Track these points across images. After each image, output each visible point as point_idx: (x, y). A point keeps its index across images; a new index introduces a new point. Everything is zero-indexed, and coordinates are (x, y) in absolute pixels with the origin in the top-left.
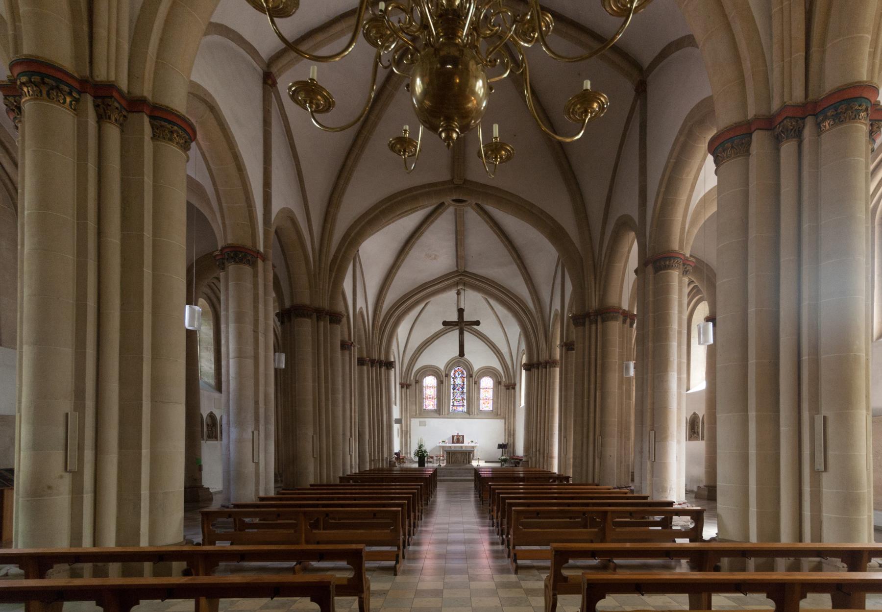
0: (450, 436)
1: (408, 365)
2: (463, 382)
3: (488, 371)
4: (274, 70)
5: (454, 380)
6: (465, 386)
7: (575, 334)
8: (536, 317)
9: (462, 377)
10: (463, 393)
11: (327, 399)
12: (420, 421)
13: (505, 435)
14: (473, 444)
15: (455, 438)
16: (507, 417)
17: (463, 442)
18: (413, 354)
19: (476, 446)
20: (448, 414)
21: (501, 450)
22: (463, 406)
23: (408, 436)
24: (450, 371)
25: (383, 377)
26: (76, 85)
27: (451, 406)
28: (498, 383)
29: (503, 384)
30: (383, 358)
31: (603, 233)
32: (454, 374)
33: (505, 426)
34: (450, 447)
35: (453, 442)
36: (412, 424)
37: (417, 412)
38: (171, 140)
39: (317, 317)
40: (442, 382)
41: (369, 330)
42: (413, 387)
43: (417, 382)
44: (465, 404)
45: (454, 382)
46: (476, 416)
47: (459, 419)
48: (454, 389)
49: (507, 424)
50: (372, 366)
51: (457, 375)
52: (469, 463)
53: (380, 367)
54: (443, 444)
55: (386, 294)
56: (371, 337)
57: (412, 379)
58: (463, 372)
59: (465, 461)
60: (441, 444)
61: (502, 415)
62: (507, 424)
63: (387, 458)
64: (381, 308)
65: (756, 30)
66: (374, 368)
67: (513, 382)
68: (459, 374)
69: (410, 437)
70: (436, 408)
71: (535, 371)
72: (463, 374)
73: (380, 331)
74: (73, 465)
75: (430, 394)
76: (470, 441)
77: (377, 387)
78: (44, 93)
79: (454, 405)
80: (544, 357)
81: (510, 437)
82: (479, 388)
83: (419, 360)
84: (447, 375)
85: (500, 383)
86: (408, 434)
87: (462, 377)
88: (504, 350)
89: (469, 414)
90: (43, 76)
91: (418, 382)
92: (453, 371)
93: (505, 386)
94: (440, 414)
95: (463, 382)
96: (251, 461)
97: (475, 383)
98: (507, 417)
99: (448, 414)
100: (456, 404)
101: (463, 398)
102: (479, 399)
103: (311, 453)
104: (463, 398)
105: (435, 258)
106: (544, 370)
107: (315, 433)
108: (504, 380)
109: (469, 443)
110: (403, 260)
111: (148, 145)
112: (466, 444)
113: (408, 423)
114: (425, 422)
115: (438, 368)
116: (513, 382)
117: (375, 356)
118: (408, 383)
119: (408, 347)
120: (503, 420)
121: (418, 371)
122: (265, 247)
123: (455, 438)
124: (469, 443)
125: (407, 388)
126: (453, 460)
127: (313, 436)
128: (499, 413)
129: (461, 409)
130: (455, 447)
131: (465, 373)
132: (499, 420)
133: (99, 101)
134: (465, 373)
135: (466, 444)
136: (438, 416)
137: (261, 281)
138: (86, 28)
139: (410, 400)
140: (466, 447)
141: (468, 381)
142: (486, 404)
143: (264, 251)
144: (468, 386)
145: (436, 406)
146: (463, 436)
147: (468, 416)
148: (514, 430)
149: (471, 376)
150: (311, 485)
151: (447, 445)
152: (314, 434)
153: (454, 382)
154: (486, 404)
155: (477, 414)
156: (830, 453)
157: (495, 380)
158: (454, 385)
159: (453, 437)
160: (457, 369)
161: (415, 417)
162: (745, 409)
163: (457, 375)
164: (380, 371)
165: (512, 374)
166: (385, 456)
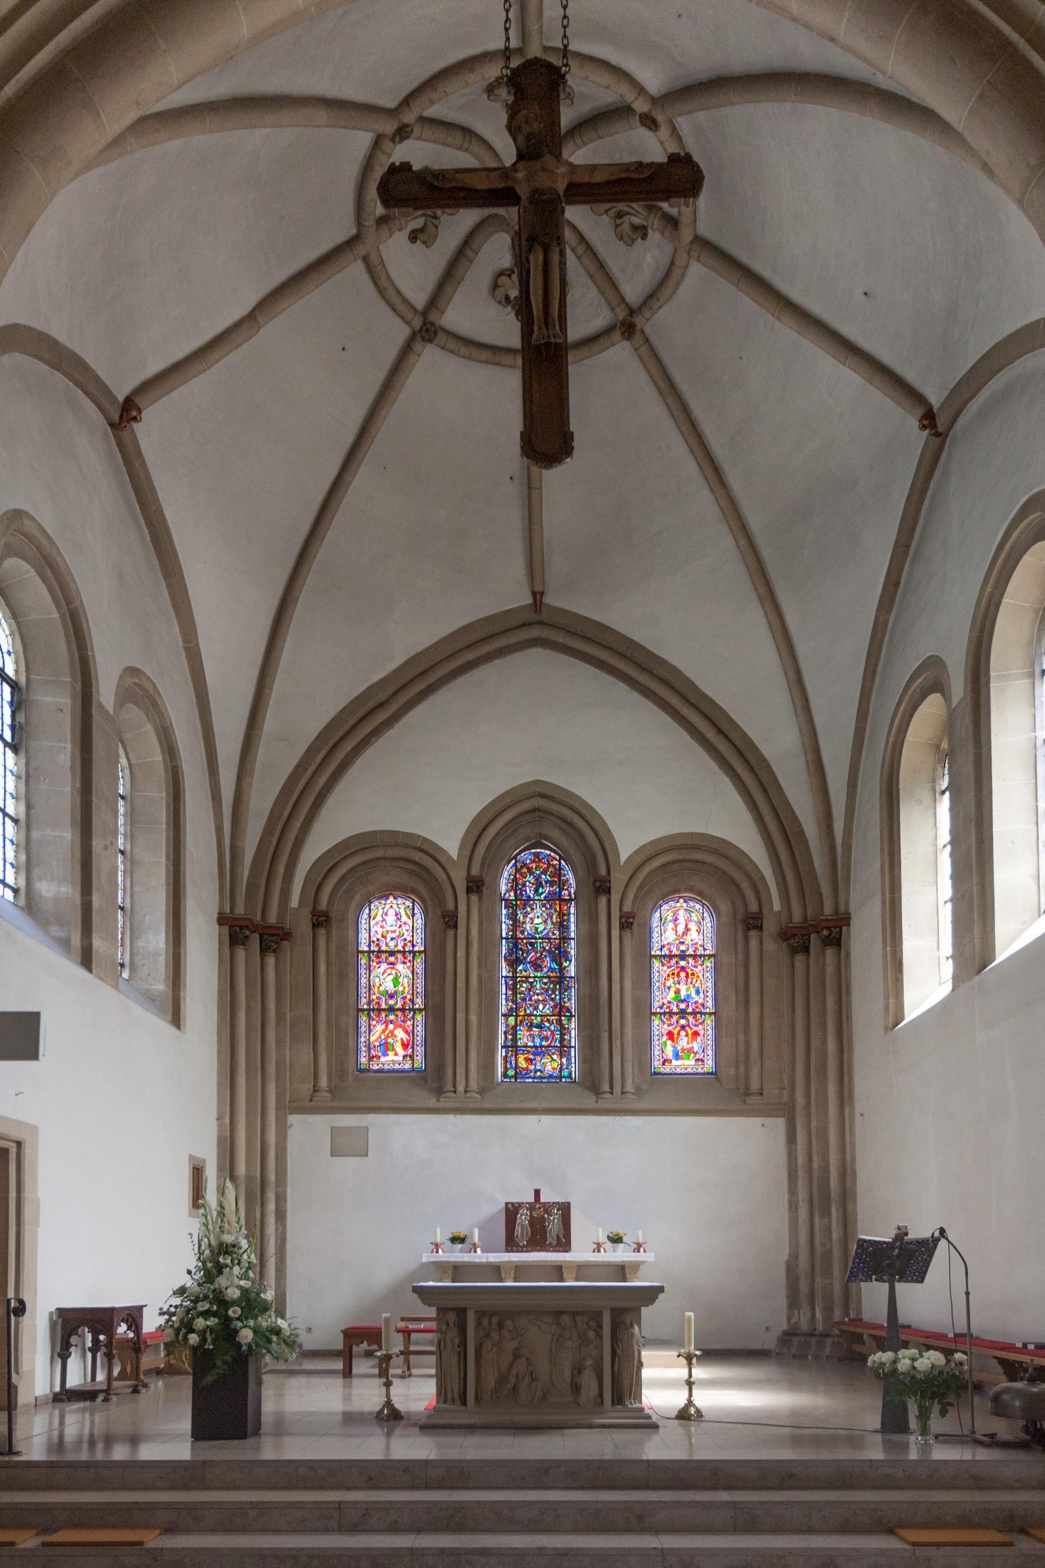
0: (494, 1207)
2: (562, 926)
4: (139, 401)
5: (513, 917)
6: (572, 948)
9: (551, 899)
10: (560, 979)
12: (334, 1130)
13: (793, 1205)
14: (620, 1255)
15: (523, 1218)
16: (800, 1099)
17: (564, 1244)
18: (300, 768)
19: (636, 1266)
20: (482, 1092)
22: (563, 1050)
23: (271, 1207)
24: (493, 862)
27: (501, 1053)
29: (770, 926)
32: (516, 885)
33: (791, 1155)
34: (496, 1271)
35: (511, 1244)
36: (292, 1146)
37: (323, 1082)
40: (450, 921)
42: (299, 950)
43: (321, 920)
44: (573, 1037)
45: (516, 924)
46: (632, 1102)
47: (546, 1119)
48: (514, 963)
51: (530, 891)
52: (618, 1399)
54: (458, 1255)
57: (294, 903)
58: (558, 873)
59: (588, 1380)
60: (442, 1256)
67: (828, 909)
68: (538, 884)
69: (281, 1216)
70: (419, 1062)
72: (562, 884)
75: (389, 986)
76: (602, 1238)
79: (513, 1047)
81: (826, 1213)
82: (644, 958)
83: (332, 801)
84: (476, 886)
85: (753, 922)
86: (271, 1196)
87: (555, 899)
89: (596, 1091)
92: (508, 871)
93: (785, 935)
94: (439, 1092)
95: (563, 926)
97: (626, 924)
98: (800, 1099)
99: (482, 1092)
100: (524, 1037)
101: (561, 1010)
102: (644, 1012)
104: (561, 1010)
108: (777, 906)
109: (598, 1247)
112: (580, 1252)
115: (428, 849)
116: (828, 909)
118: (273, 919)
119: (269, 725)
120: (781, 1123)
123: (523, 1218)
124: (598, 1247)
125: (264, 949)
126: (491, 1383)
128: (755, 1086)
129: (550, 1065)
130: (520, 1271)
131: (570, 877)
132: (757, 1121)
134: (570, 877)
135: (580, 1252)
136: (432, 1102)
139: (280, 1018)
140: (582, 1269)
141: (589, 918)
142: (683, 1042)
144: (590, 942)
145: (420, 1051)
146: (565, 1209)
147: (590, 1100)
148: (847, 1173)
149: (601, 887)
151: (480, 1257)
153: (516, 924)
154: (683, 1042)
155: (638, 1091)
157: (725, 907)
158: (514, 940)
159: (511, 1211)
160: (526, 857)
161: (310, 1106)
163: (530, 891)
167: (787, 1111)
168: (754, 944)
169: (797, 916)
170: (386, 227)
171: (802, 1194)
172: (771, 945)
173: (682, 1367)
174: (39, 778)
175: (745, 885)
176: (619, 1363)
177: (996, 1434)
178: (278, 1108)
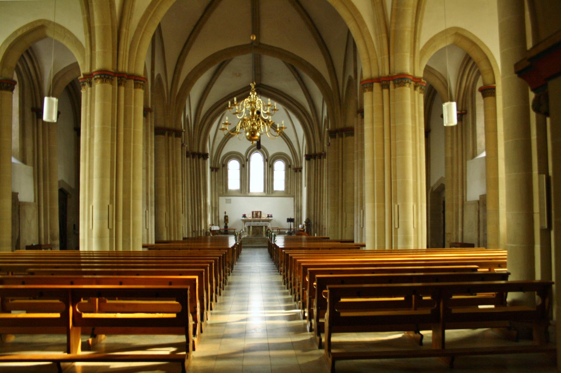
1: (217, 150)
3: (279, 156)
7: (351, 121)
8: (312, 118)
11: (173, 188)
13: (294, 211)
15: (254, 213)
16: (295, 195)
17: (260, 217)
21: (289, 223)
25: (201, 166)
26: (112, 74)
28: (288, 167)
29: (292, 167)
30: (201, 151)
31: (344, 80)
38: (140, 87)
39: (168, 134)
41: (191, 127)
42: (220, 171)
49: (295, 201)
50: (193, 157)
53: (199, 158)
55: (204, 103)
56: (193, 135)
61: (292, 193)
62: (295, 201)
63: (204, 230)
64: (201, 112)
65: (372, 42)
66: (195, 159)
67: (300, 166)
71: (313, 160)
73: (199, 130)
74: (110, 227)
77: (197, 174)
78: (104, 81)
80: (318, 151)
85: (290, 166)
88: (293, 139)
90: (105, 75)
91: (225, 166)
96: (145, 228)
98: (295, 195)
103: (165, 225)
105: (239, 76)
106: (319, 160)
107: (167, 211)
108: (293, 164)
110: (217, 78)
111: (133, 92)
113: (217, 201)
114: (230, 200)
116: (300, 166)
117: (196, 150)
119: (217, 136)
121: (225, 157)
122: (151, 104)
123: (254, 213)
125: (216, 171)
127: (166, 213)
133: (119, 79)
137: (149, 124)
138: (116, 52)
143: (151, 107)
146: (261, 212)
150: (184, 239)
152: (166, 212)
156: (400, 220)
159: (253, 212)
161: (222, 195)
162: (374, 202)
164: (199, 162)
165: (299, 158)
166: (203, 228)
167: (294, 197)
168: (289, 170)
169: (295, 166)
170: (273, 264)
171: (295, 210)
172: (292, 170)
173: (414, 247)
174: (122, 84)
175: (288, 160)
176: (233, 322)
177: (236, 229)
178: (218, 196)
